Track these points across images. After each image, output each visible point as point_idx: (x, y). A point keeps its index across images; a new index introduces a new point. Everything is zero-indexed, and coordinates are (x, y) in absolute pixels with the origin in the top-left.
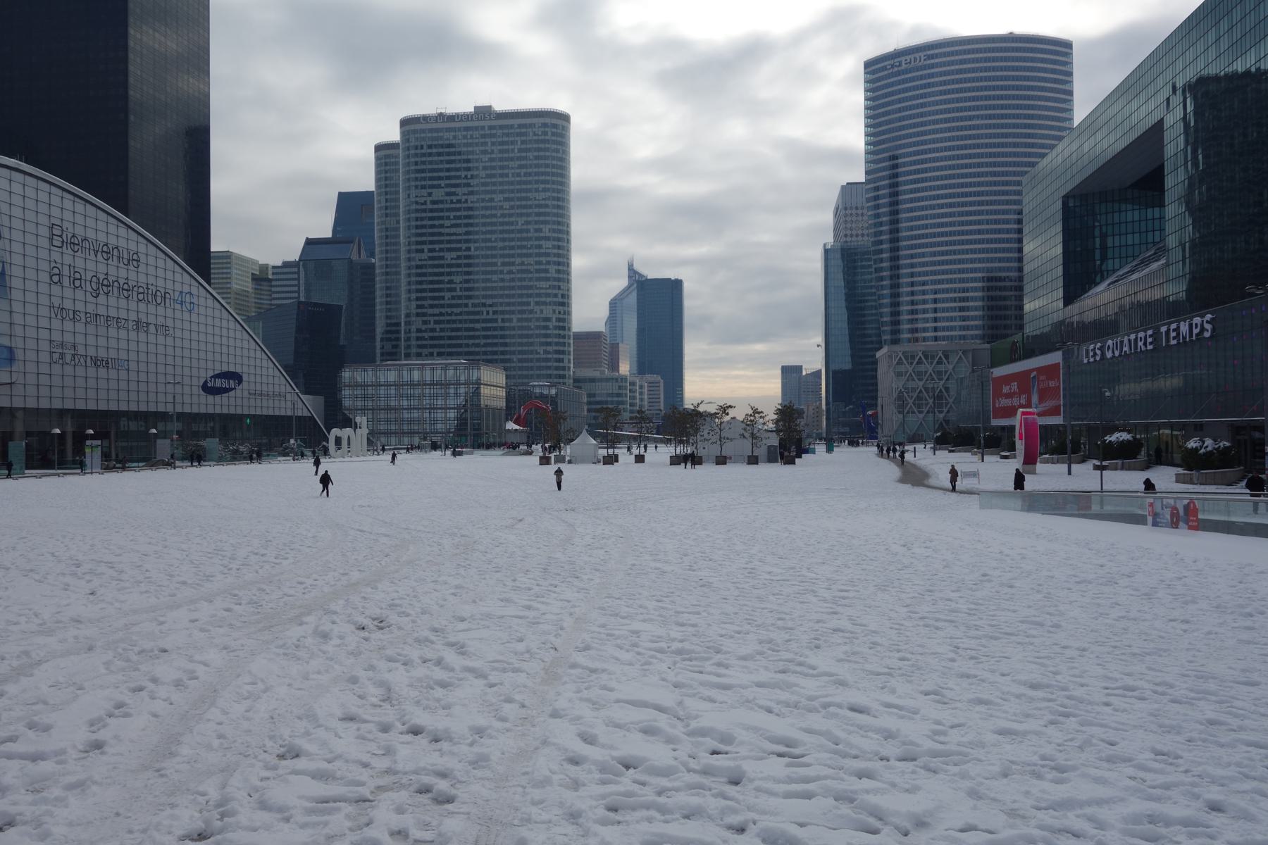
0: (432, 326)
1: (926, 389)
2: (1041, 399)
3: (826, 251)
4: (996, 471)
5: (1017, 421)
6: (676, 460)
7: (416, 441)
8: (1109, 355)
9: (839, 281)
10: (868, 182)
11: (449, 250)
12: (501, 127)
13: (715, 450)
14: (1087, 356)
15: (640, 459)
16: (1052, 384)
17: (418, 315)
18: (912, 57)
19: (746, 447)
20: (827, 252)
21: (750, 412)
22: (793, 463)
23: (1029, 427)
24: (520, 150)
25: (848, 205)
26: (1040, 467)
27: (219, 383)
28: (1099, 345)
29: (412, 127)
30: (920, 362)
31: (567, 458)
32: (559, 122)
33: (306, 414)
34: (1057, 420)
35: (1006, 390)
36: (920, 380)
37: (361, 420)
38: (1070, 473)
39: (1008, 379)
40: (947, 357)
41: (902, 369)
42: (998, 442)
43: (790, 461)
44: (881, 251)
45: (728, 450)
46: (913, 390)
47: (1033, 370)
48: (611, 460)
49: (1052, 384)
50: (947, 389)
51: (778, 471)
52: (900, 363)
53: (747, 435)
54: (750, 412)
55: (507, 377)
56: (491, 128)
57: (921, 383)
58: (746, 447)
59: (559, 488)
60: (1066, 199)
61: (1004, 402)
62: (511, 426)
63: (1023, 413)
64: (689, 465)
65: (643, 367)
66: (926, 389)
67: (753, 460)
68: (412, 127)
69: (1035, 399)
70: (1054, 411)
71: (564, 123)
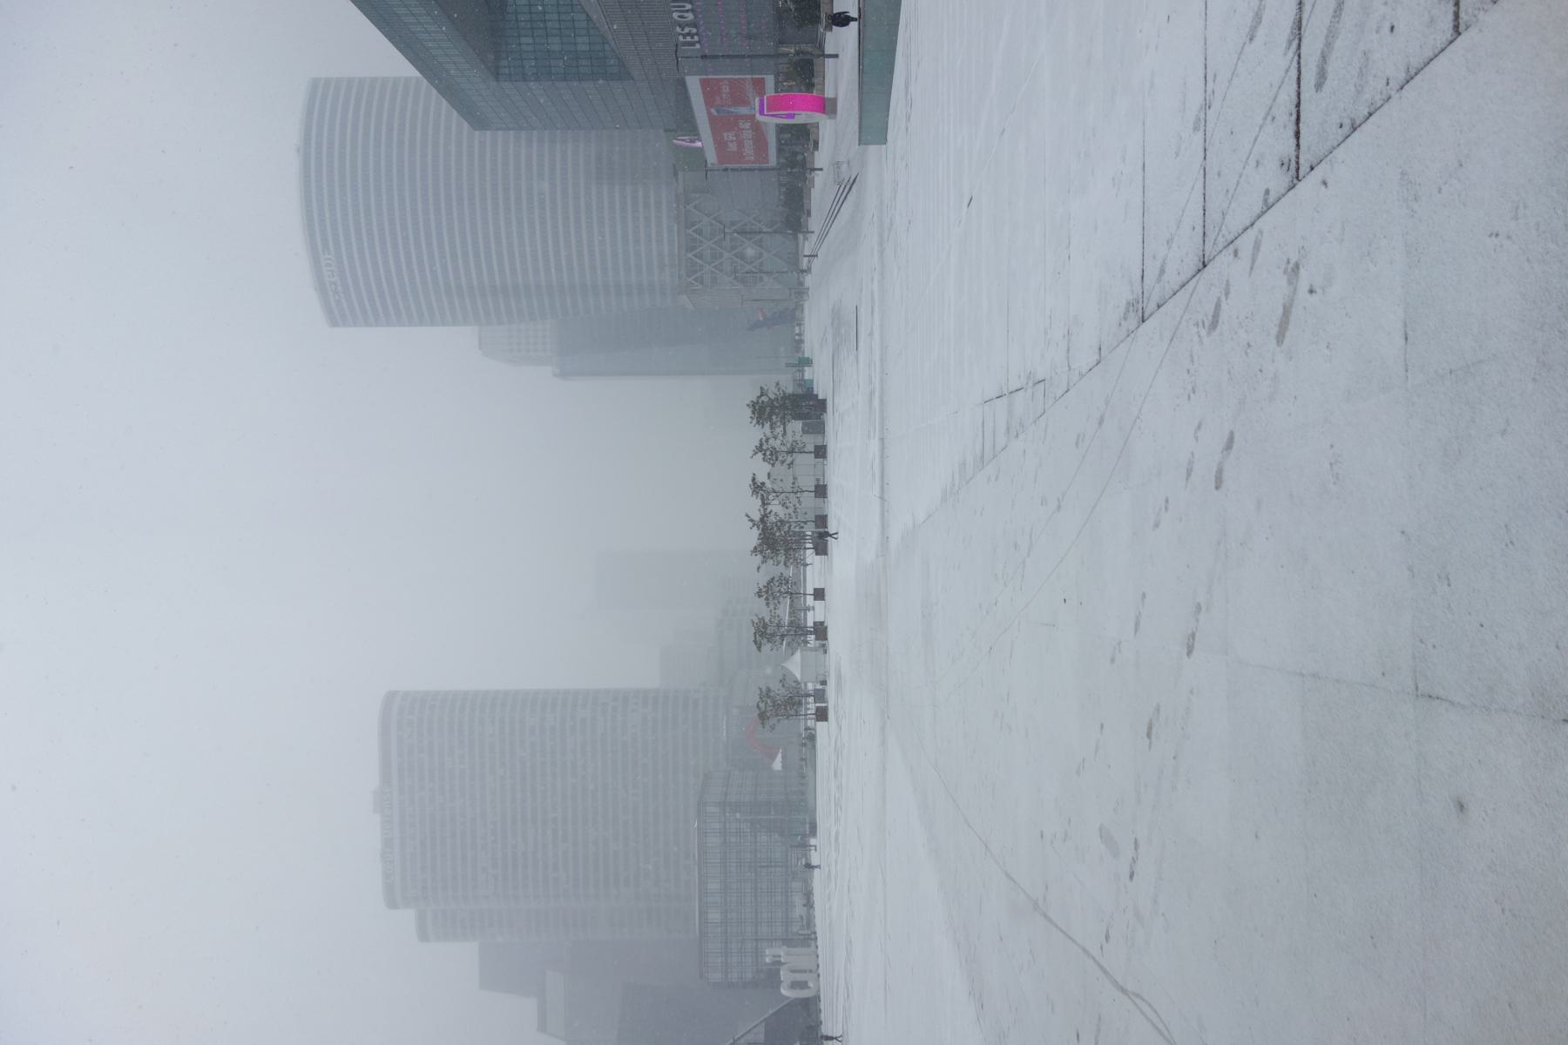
2: (745, 102)
4: (834, 137)
5: (770, 122)
6: (821, 550)
7: (796, 885)
8: (690, 16)
13: (809, 501)
14: (693, 44)
15: (819, 594)
16: (726, 89)
19: (805, 461)
20: (564, 374)
21: (760, 455)
22: (823, 402)
23: (776, 105)
26: (829, 94)
28: (678, 29)
30: (700, 256)
31: (819, 687)
33: (762, 1029)
34: (770, 81)
35: (733, 147)
36: (721, 255)
37: (768, 956)
38: (836, 56)
39: (720, 145)
42: (799, 141)
43: (822, 405)
45: (808, 483)
47: (709, 113)
48: (821, 631)
49: (726, 89)
51: (830, 419)
53: (789, 459)
54: (760, 455)
57: (726, 255)
58: (805, 461)
61: (749, 150)
62: (777, 765)
63: (761, 112)
64: (813, 841)
66: (733, 248)
67: (821, 452)
69: (743, 110)
70: (759, 85)
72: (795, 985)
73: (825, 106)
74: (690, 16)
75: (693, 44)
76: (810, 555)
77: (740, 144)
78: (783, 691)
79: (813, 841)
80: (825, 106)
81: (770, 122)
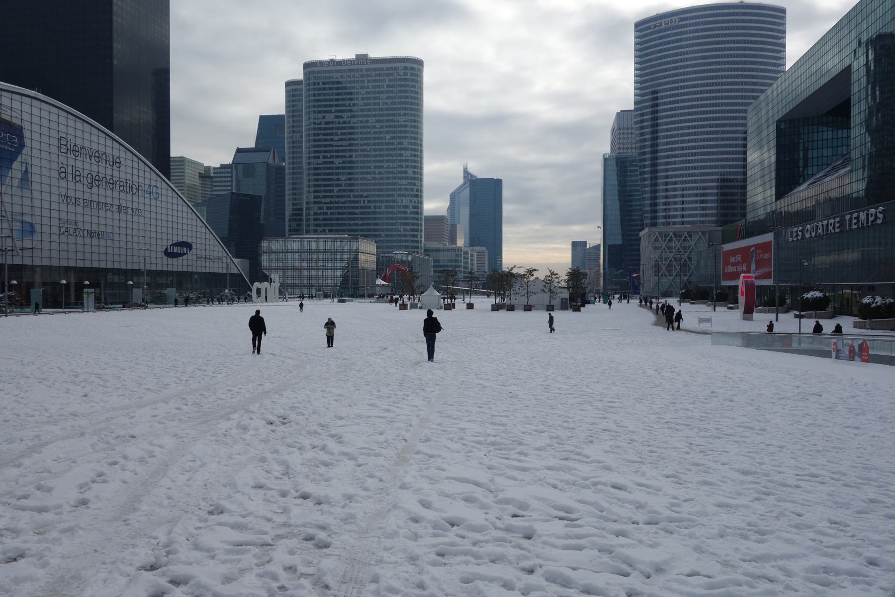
0: (325, 210)
1: (675, 259)
2: (758, 267)
3: (605, 160)
8: (807, 235)
9: (614, 181)
10: (636, 110)
11: (337, 157)
12: (375, 69)
13: (524, 301)
14: (792, 236)
15: (470, 306)
16: (766, 256)
17: (315, 203)
18: (669, 19)
21: (549, 274)
23: (749, 287)
24: (388, 86)
25: (622, 127)
26: (755, 315)
27: (176, 250)
29: (311, 69)
32: (416, 66)
33: (236, 272)
34: (769, 282)
35: (732, 260)
36: (671, 252)
37: (274, 276)
39: (734, 252)
40: (690, 236)
41: (658, 244)
43: (577, 309)
44: (645, 160)
45: (533, 300)
46: (666, 259)
47: (752, 246)
49: (766, 256)
50: (690, 259)
52: (656, 240)
53: (546, 290)
54: (549, 274)
55: (377, 247)
56: (367, 70)
57: (671, 255)
58: (545, 298)
59: (330, 341)
60: (779, 123)
61: (731, 269)
65: (473, 241)
66: (675, 259)
68: (311, 69)
69: (753, 267)
70: (767, 276)
71: (419, 67)
72: (259, 291)
73: (748, 311)
74: (807, 235)
75: (792, 236)
76: (492, 300)
77: (735, 264)
78: (416, 285)
79: (336, 300)
80: (748, 311)
81: (740, 282)
